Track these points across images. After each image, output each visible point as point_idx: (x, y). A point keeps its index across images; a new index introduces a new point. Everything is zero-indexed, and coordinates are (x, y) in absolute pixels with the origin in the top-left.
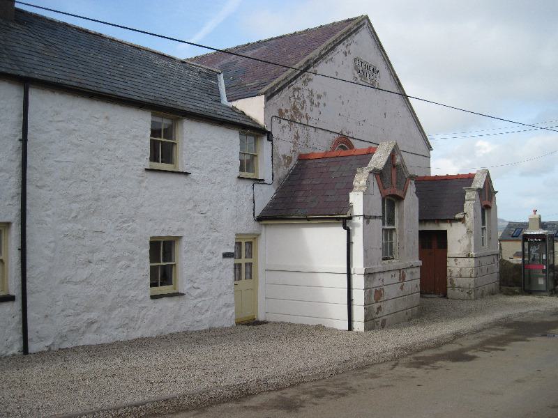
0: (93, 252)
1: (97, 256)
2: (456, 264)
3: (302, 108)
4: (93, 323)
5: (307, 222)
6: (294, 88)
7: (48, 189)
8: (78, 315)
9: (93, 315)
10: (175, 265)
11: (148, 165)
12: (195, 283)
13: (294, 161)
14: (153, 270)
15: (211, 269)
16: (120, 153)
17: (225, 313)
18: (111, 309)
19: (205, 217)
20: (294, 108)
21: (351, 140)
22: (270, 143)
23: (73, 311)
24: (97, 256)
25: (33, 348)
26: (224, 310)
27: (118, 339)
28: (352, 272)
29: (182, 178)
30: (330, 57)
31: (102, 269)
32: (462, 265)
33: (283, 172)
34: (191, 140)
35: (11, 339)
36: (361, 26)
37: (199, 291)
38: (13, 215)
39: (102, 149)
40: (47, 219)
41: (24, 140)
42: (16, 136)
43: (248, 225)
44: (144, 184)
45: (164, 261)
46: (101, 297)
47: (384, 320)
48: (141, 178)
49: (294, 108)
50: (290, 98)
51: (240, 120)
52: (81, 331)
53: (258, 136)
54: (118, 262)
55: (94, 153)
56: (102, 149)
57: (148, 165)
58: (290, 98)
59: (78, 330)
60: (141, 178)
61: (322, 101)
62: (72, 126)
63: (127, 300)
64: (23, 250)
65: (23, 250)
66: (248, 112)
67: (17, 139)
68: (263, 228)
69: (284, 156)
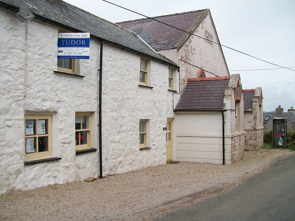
0: (121, 127)
1: (124, 128)
2: (248, 133)
3: (189, 55)
4: (121, 162)
5: (203, 112)
6: (186, 46)
7: (107, 95)
8: (116, 158)
9: (120, 159)
10: (146, 133)
11: (56, 69)
12: (154, 142)
13: (186, 82)
14: (77, 133)
15: (159, 135)
16: (130, 77)
17: (163, 158)
18: (127, 155)
19: (158, 109)
20: (186, 55)
21: (204, 71)
22: (179, 72)
23: (114, 156)
24: (124, 128)
25: (104, 174)
26: (163, 156)
27: (129, 170)
28: (225, 136)
29: (149, 90)
30: (197, 30)
31: (124, 135)
32: (251, 134)
33: (183, 87)
34: (153, 71)
35: (95, 170)
36: (207, 14)
37: (155, 146)
38: (94, 108)
39: (125, 75)
40: (107, 110)
41: (100, 70)
42: (96, 68)
43: (171, 114)
44: (138, 93)
45: (83, 128)
46: (124, 149)
47: (235, 159)
48: (137, 90)
49: (186, 55)
50: (185, 50)
51: (163, 59)
52: (117, 167)
53: (173, 69)
54: (129, 132)
55: (122, 77)
56: (125, 75)
57: (56, 69)
58: (185, 50)
59: (116, 166)
60: (137, 90)
61: (195, 52)
62: (115, 63)
63: (132, 151)
64: (100, 126)
65: (100, 126)
66: (167, 57)
67: (97, 69)
68: (176, 116)
69: (183, 79)
